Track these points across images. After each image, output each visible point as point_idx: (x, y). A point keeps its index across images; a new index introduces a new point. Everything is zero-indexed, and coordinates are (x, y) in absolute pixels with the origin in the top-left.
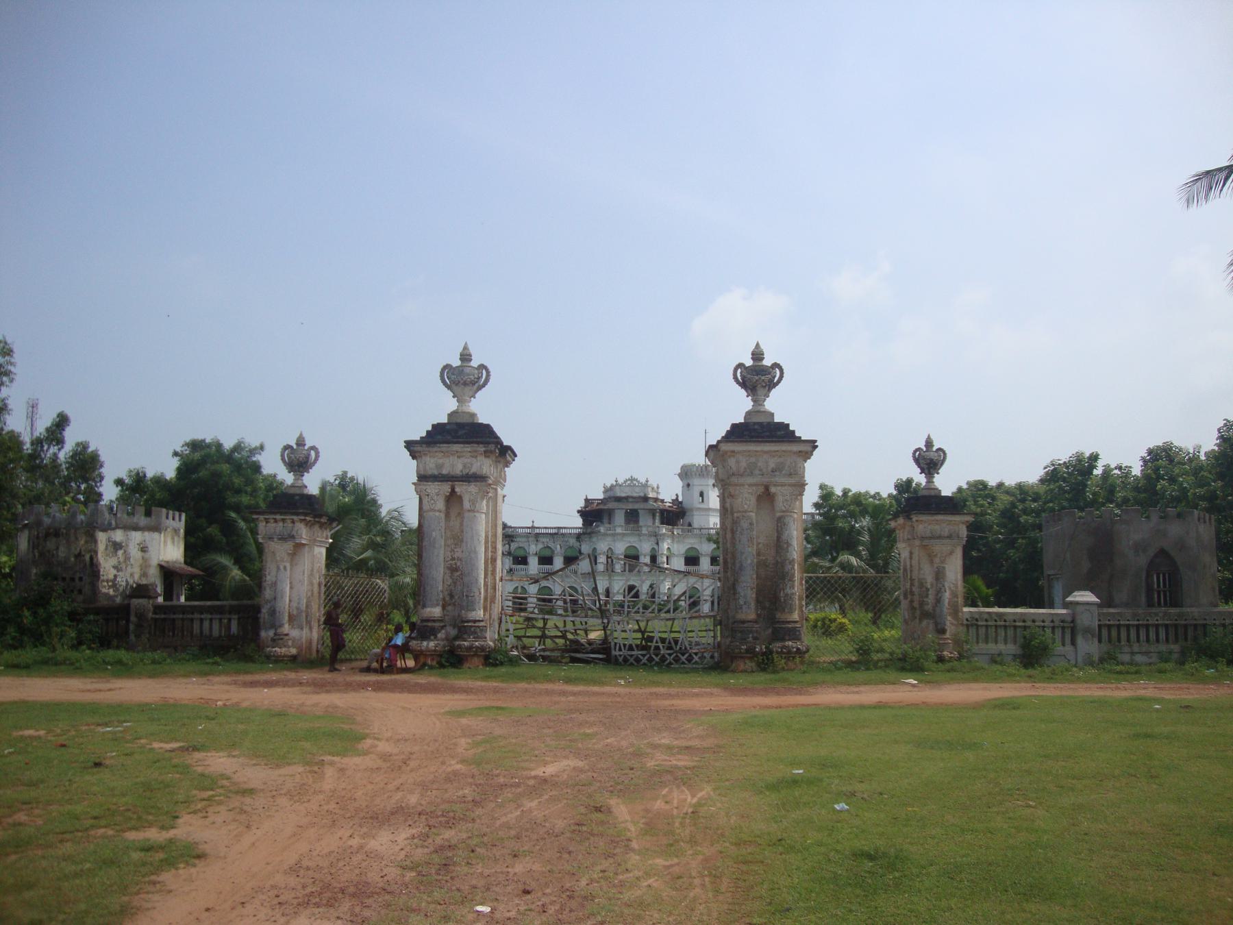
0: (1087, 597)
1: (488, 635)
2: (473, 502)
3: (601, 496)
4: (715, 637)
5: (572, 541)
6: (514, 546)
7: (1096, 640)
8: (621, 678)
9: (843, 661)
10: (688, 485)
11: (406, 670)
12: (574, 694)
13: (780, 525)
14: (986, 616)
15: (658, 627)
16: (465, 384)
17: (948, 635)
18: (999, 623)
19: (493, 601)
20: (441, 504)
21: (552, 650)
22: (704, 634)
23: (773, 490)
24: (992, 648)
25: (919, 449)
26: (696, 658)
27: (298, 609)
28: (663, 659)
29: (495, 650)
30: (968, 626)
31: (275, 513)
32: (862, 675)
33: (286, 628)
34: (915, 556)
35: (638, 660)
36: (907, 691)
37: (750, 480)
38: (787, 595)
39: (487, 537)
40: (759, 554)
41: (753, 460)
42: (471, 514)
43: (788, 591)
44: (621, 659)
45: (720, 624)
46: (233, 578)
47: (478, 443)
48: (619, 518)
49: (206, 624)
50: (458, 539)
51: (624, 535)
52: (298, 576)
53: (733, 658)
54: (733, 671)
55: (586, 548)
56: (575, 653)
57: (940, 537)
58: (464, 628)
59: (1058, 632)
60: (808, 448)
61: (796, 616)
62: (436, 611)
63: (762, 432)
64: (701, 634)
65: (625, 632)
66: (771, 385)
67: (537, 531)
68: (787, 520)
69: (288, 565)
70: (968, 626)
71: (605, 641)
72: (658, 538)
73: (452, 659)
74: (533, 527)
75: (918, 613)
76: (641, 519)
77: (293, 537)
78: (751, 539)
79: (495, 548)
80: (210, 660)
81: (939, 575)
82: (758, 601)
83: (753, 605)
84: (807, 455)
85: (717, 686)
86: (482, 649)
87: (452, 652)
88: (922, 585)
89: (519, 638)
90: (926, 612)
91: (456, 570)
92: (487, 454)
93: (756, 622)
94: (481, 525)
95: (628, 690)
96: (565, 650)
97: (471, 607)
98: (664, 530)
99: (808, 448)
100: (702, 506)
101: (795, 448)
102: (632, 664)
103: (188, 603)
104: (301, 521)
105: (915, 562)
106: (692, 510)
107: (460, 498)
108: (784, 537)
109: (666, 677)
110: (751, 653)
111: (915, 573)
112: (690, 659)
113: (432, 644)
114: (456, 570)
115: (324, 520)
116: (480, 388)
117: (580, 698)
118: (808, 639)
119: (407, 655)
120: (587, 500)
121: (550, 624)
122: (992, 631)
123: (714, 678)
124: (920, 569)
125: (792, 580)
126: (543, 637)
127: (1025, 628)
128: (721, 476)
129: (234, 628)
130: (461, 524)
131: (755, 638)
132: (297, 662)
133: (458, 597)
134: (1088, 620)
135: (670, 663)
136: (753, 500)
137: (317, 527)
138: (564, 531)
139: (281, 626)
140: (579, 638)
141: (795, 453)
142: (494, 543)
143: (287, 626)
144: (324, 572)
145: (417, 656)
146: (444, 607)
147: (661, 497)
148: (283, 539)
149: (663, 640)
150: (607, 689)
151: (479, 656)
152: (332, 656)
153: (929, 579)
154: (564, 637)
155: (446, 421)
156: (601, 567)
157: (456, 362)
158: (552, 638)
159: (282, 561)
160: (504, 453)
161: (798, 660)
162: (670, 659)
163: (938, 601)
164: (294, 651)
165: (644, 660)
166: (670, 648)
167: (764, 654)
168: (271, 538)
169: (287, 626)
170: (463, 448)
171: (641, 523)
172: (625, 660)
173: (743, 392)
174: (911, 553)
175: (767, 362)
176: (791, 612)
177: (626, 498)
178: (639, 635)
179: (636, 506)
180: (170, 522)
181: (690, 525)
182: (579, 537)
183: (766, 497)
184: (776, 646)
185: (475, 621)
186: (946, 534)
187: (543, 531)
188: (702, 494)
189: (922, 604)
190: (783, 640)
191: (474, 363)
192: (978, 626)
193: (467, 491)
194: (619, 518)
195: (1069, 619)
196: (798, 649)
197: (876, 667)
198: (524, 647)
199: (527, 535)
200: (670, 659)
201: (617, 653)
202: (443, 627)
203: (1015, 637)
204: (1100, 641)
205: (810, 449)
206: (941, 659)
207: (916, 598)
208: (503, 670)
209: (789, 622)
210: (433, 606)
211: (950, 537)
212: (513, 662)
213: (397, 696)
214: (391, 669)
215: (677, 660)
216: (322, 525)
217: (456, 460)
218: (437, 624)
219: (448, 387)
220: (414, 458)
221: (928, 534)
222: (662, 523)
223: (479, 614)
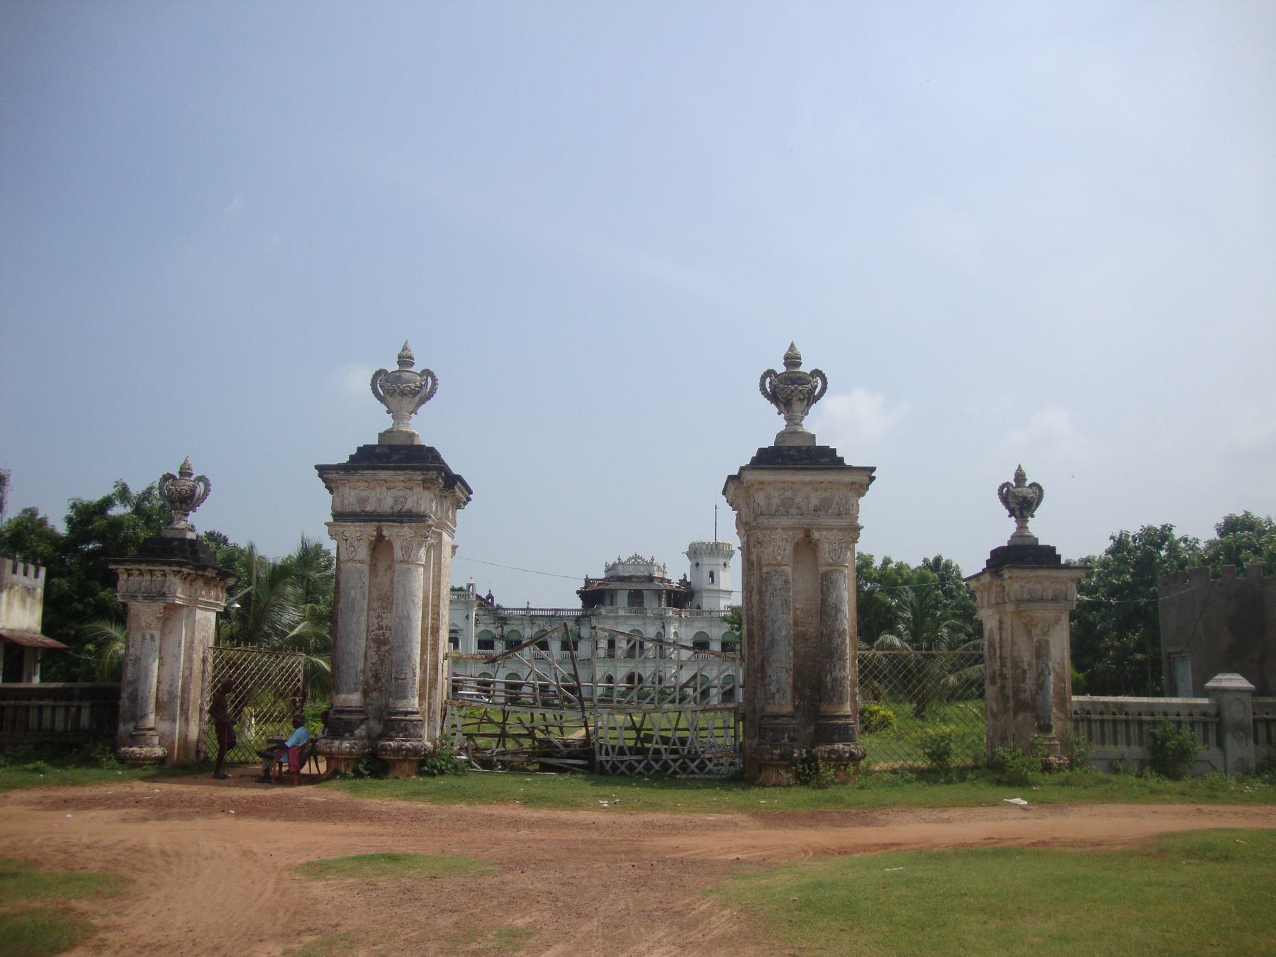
0: (1235, 681)
1: (425, 732)
2: (407, 550)
3: (603, 576)
4: (736, 736)
5: (571, 625)
6: (507, 629)
7: (1251, 741)
8: (603, 797)
9: (911, 770)
10: (697, 565)
11: (313, 780)
12: (530, 825)
13: (826, 583)
14: (1100, 708)
15: (661, 721)
16: (403, 394)
17: (1053, 734)
18: (1119, 717)
19: (433, 686)
20: (363, 553)
21: (515, 753)
22: (722, 732)
23: (816, 535)
24: (1111, 751)
25: (1007, 484)
26: (710, 766)
27: (170, 693)
28: (665, 767)
29: (433, 754)
30: (1076, 721)
31: (140, 562)
32: (942, 791)
33: (151, 719)
34: (1007, 626)
35: (631, 768)
36: (1013, 818)
37: (785, 522)
38: (835, 679)
39: (425, 598)
40: (796, 624)
41: (788, 494)
42: (404, 566)
43: (837, 673)
44: (608, 767)
45: (744, 718)
46: (116, 652)
47: (414, 469)
48: (622, 599)
49: (47, 714)
50: (387, 600)
51: (627, 617)
52: (176, 650)
53: (762, 767)
54: (763, 785)
55: (585, 632)
56: (547, 757)
57: (1042, 600)
58: (393, 723)
59: (1198, 731)
60: (863, 478)
61: (847, 709)
62: (355, 699)
63: (795, 457)
64: (716, 732)
65: (612, 727)
66: (812, 398)
67: (533, 613)
68: (834, 576)
69: (157, 634)
70: (1076, 721)
71: (587, 741)
72: (664, 621)
73: (376, 765)
74: (528, 609)
75: (1011, 704)
76: (645, 601)
77: (164, 595)
78: (785, 602)
79: (437, 615)
80: (31, 766)
81: (1041, 652)
82: (795, 688)
83: (789, 691)
84: (861, 489)
85: (742, 809)
86: (415, 751)
87: (377, 753)
88: (1016, 664)
89: (470, 736)
90: (1021, 704)
91: (384, 642)
92: (427, 484)
93: (792, 716)
94: (419, 582)
95: (612, 817)
96: (532, 754)
97: (402, 694)
98: (670, 612)
99: (863, 478)
100: (712, 587)
101: (847, 478)
102: (623, 773)
103: (44, 685)
104: (176, 573)
105: (1007, 635)
106: (700, 591)
107: (390, 545)
108: (831, 600)
109: (668, 795)
110: (787, 760)
111: (1007, 648)
112: (701, 767)
113: (346, 744)
114: (384, 642)
115: (210, 573)
116: (423, 401)
117: (538, 834)
118: (864, 742)
119: (319, 757)
120: (587, 581)
121: (512, 719)
122: (1109, 728)
123: (735, 796)
124: (1013, 644)
125: (841, 658)
126: (503, 736)
127: (1155, 723)
128: (744, 519)
129: (85, 720)
130: (392, 581)
131: (792, 739)
132: (166, 768)
133: (385, 678)
134: (1236, 713)
135: (675, 772)
136: (789, 548)
137: (200, 583)
138: (562, 613)
139: (144, 716)
140: (552, 737)
141: (845, 485)
142: (436, 608)
143: (152, 717)
144: (211, 644)
145: (330, 758)
146: (366, 694)
147: (667, 577)
148: (150, 597)
149: (665, 740)
150: (582, 815)
151: (411, 761)
152: (206, 764)
153: (1026, 656)
154: (531, 735)
155: (376, 443)
156: (602, 653)
157: (392, 367)
158: (515, 736)
159: (149, 627)
160: (452, 487)
161: (851, 769)
162: (675, 766)
163: (1041, 686)
164: (159, 751)
165: (640, 768)
166: (674, 752)
167: (804, 761)
168: (134, 597)
169: (152, 717)
170: (399, 479)
171: (646, 606)
172: (614, 768)
173: (773, 409)
174: (1001, 622)
175: (806, 368)
176: (841, 702)
177: (630, 578)
178: (633, 734)
179: (639, 587)
180: (19, 577)
181: (699, 607)
182: (578, 620)
183: (807, 545)
184: (822, 749)
185: (407, 713)
186: (1051, 595)
187: (540, 613)
188: (712, 575)
189: (1017, 691)
190: (832, 742)
191: (417, 368)
192: (1089, 721)
193: (398, 534)
194: (622, 599)
195: (1213, 711)
196: (852, 754)
197: (962, 779)
198: (477, 749)
199: (522, 617)
200: (675, 766)
201: (604, 758)
202: (362, 721)
203: (1141, 736)
204: (1256, 742)
205: (866, 479)
206: (1047, 768)
207: (1009, 683)
208: (442, 781)
209: (838, 717)
210: (350, 691)
211: (1055, 599)
212: (458, 770)
213: (266, 824)
214: (294, 778)
215: (684, 768)
216: (208, 582)
217: (383, 492)
218: (355, 717)
219: (382, 400)
220: (331, 492)
221: (1026, 596)
222: (669, 605)
223: (414, 703)
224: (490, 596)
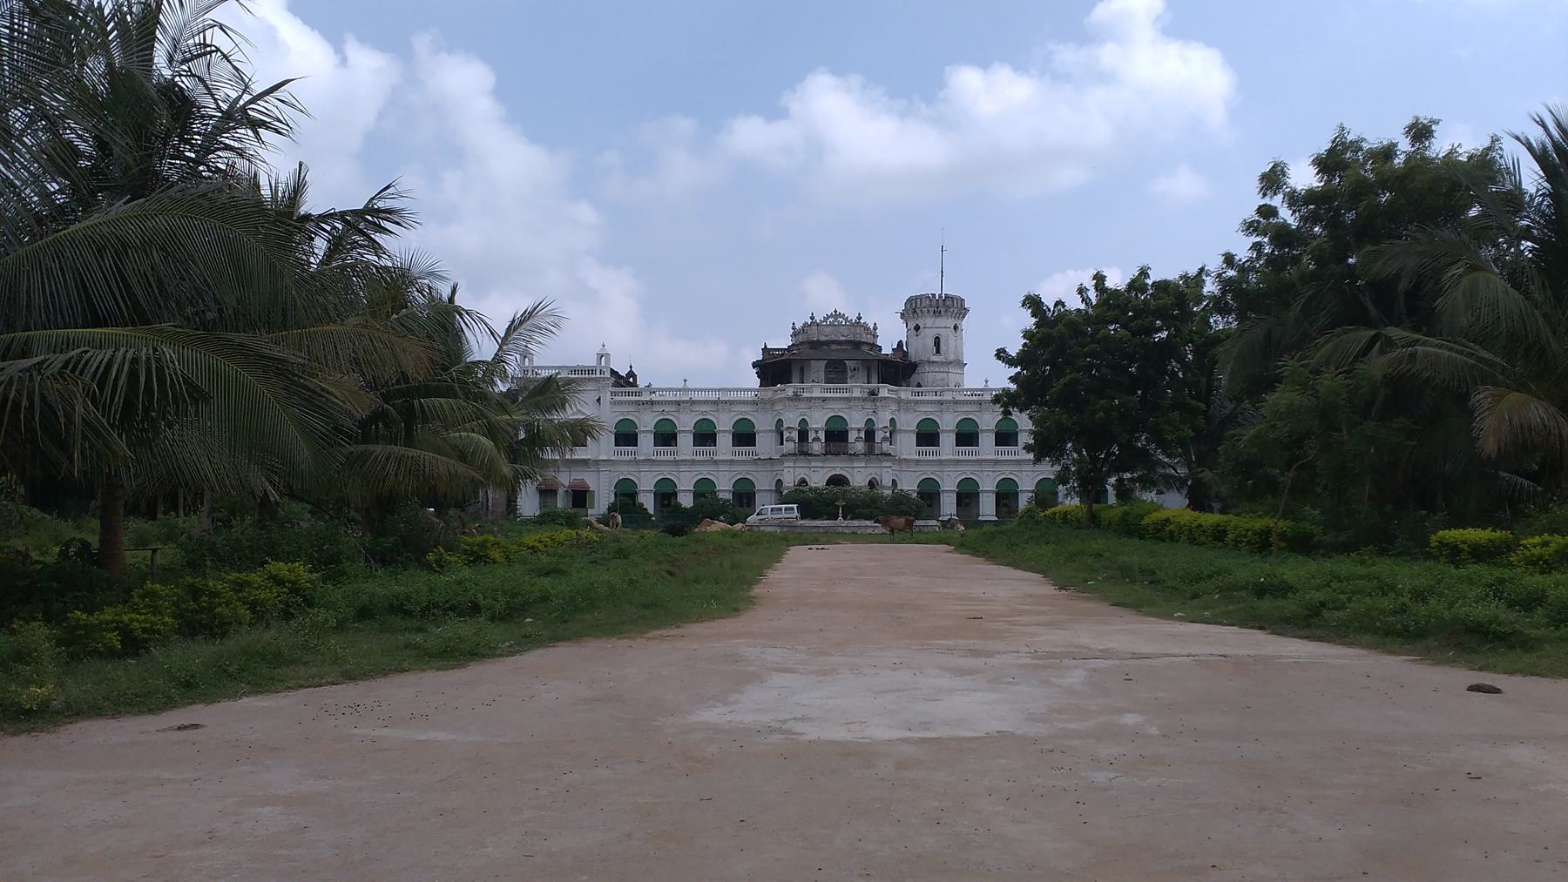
10: (917, 328)
120: (765, 350)
194: (818, 369)
224: (631, 374)
